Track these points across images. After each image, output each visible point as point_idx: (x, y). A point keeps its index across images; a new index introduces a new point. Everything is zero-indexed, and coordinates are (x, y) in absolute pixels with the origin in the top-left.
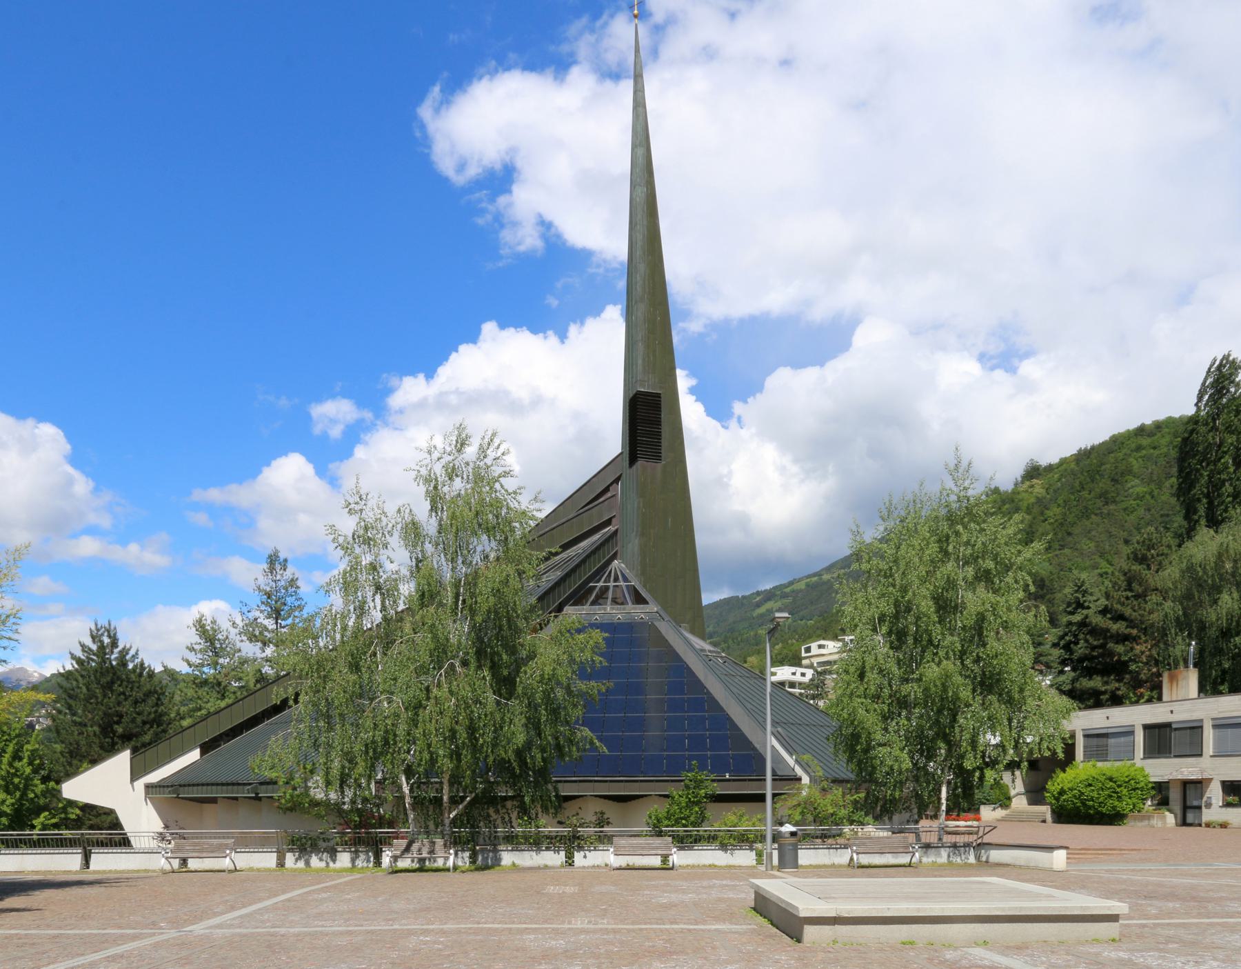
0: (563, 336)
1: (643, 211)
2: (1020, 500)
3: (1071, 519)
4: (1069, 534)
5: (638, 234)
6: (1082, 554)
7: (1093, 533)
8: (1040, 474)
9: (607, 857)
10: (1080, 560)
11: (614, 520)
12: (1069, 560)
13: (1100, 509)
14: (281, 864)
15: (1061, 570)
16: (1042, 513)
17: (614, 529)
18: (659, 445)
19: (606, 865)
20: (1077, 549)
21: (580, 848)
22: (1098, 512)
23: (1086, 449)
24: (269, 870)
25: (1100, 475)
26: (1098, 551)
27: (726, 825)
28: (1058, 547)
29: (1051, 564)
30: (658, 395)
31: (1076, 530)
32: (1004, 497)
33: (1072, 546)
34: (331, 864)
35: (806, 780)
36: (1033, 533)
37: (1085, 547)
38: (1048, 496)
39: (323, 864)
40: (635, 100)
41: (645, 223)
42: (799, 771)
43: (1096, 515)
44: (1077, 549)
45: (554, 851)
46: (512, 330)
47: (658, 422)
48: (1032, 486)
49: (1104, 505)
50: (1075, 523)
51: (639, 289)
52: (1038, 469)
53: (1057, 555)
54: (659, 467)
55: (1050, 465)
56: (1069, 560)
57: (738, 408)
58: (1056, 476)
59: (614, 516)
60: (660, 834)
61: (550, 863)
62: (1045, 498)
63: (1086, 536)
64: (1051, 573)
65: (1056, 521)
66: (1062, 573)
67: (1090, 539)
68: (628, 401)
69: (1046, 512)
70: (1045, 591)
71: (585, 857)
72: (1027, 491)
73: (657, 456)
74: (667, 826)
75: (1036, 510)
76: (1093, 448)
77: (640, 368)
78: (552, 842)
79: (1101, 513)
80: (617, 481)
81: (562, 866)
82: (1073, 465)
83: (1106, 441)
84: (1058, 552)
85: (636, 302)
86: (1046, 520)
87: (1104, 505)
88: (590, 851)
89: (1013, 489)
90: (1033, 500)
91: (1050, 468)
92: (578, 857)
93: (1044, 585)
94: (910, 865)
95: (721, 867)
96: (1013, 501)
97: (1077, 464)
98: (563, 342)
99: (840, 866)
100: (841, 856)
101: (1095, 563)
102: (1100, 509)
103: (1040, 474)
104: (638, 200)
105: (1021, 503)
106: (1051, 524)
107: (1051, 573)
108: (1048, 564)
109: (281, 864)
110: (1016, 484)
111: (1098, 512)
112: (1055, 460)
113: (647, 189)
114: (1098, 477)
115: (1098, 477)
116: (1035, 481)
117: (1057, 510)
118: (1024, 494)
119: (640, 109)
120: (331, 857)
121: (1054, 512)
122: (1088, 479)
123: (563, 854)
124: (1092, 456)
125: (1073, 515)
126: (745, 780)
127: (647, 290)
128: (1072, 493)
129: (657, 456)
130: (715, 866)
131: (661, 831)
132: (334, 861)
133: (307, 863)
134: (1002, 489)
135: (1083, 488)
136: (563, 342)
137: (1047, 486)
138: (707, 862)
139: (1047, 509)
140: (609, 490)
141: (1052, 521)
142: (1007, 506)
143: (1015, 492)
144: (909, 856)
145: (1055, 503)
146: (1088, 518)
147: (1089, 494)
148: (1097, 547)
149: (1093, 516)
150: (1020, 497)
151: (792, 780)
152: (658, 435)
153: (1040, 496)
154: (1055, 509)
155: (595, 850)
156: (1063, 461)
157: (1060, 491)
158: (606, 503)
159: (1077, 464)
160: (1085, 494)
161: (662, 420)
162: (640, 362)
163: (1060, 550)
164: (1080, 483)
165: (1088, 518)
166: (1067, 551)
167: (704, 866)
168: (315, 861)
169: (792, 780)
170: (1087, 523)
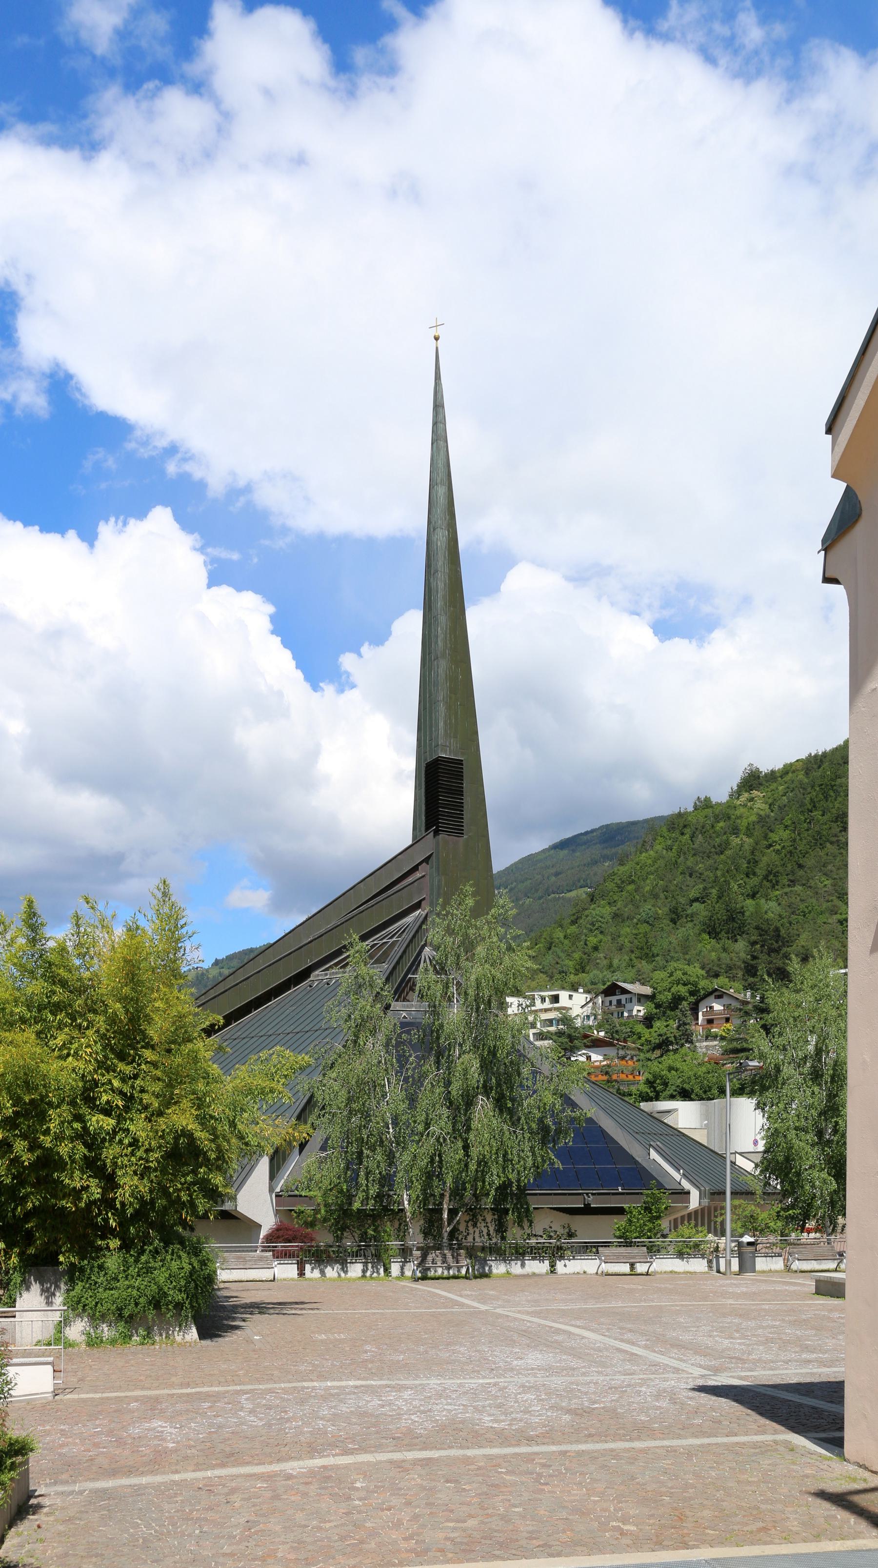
0: (89, 537)
1: (445, 557)
2: (740, 817)
3: (801, 847)
4: (800, 866)
5: (439, 583)
6: (817, 893)
7: (830, 867)
8: (761, 784)
9: (588, 1265)
10: (814, 900)
11: (423, 903)
12: (801, 900)
13: (836, 836)
14: (301, 1273)
15: (793, 913)
16: (766, 837)
17: (424, 913)
18: (460, 817)
19: (585, 1272)
20: (810, 887)
21: (562, 1258)
22: (834, 839)
23: (816, 756)
24: (292, 1280)
25: (834, 791)
26: (836, 891)
27: (683, 1237)
28: (786, 882)
29: (779, 904)
30: (460, 762)
31: (809, 862)
32: (717, 812)
33: (804, 882)
34: (343, 1275)
35: (695, 1195)
36: (757, 862)
37: (820, 885)
38: (772, 814)
39: (336, 1275)
40: (435, 431)
41: (447, 570)
42: (686, 1185)
43: (832, 843)
44: (810, 887)
45: (540, 1260)
46: (19, 525)
47: (460, 792)
48: (751, 800)
49: (841, 831)
50: (807, 853)
51: (440, 643)
52: (759, 777)
53: (786, 894)
54: (461, 841)
55: (773, 772)
56: (801, 900)
57: (348, 661)
58: (781, 788)
59: (424, 899)
60: (629, 1244)
61: (537, 1271)
62: (768, 816)
63: (820, 871)
64: (780, 916)
65: (784, 847)
66: (793, 917)
67: (825, 874)
68: (424, 765)
69: (771, 835)
70: (780, 943)
71: (565, 1266)
72: (745, 806)
73: (458, 831)
74: (636, 1238)
75: (758, 832)
76: (825, 754)
77: (441, 731)
78: (537, 1253)
79: (838, 841)
80: (427, 860)
81: (547, 1274)
82: (801, 776)
83: (840, 746)
84: (787, 890)
85: (437, 658)
86: (770, 846)
87: (841, 831)
88: (569, 1260)
89: (727, 802)
90: (754, 818)
91: (772, 776)
92: (559, 1265)
93: (779, 936)
94: (647, 1274)
95: (679, 1273)
96: (729, 818)
97: (807, 774)
98: (91, 545)
99: (776, 1271)
100: (776, 1263)
101: (834, 906)
102: (836, 836)
103: (761, 784)
104: (439, 544)
105: (739, 821)
106: (778, 852)
107: (780, 916)
108: (776, 904)
109: (301, 1273)
110: (731, 796)
111: (834, 839)
112: (778, 765)
113: (449, 531)
114: (832, 793)
115: (832, 793)
116: (755, 793)
117: (785, 834)
118: (742, 810)
119: (441, 443)
120: (343, 1269)
121: (781, 835)
122: (821, 796)
123: (547, 1262)
124: (826, 765)
125: (805, 842)
126: (638, 1194)
127: (449, 645)
128: (802, 812)
129: (458, 831)
130: (676, 1272)
131: (632, 1242)
132: (346, 1272)
133: (323, 1273)
134: (714, 800)
135: (814, 806)
136: (91, 545)
137: (770, 801)
138: (669, 1269)
139: (772, 831)
140: (417, 869)
141: (778, 847)
142: (722, 824)
143: (729, 805)
144: (836, 1262)
145: (782, 823)
146: (822, 847)
147: (823, 815)
148: (834, 885)
149: (828, 845)
150: (738, 813)
151: (680, 1193)
152: (460, 807)
153: (762, 813)
154: (781, 832)
155: (574, 1259)
156: (788, 769)
157: (787, 808)
158: (416, 884)
159: (807, 774)
160: (817, 814)
161: (464, 790)
162: (441, 724)
163: (789, 886)
164: (811, 799)
165: (822, 847)
166: (798, 888)
167: (665, 1272)
168: (331, 1272)
169: (680, 1193)
170: (822, 853)
